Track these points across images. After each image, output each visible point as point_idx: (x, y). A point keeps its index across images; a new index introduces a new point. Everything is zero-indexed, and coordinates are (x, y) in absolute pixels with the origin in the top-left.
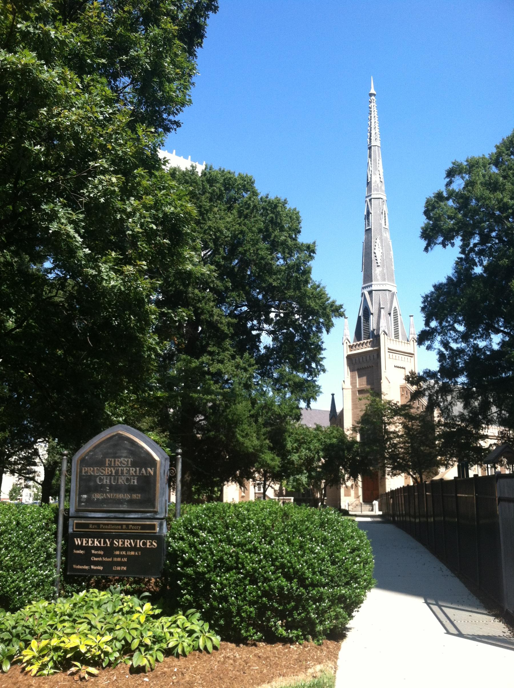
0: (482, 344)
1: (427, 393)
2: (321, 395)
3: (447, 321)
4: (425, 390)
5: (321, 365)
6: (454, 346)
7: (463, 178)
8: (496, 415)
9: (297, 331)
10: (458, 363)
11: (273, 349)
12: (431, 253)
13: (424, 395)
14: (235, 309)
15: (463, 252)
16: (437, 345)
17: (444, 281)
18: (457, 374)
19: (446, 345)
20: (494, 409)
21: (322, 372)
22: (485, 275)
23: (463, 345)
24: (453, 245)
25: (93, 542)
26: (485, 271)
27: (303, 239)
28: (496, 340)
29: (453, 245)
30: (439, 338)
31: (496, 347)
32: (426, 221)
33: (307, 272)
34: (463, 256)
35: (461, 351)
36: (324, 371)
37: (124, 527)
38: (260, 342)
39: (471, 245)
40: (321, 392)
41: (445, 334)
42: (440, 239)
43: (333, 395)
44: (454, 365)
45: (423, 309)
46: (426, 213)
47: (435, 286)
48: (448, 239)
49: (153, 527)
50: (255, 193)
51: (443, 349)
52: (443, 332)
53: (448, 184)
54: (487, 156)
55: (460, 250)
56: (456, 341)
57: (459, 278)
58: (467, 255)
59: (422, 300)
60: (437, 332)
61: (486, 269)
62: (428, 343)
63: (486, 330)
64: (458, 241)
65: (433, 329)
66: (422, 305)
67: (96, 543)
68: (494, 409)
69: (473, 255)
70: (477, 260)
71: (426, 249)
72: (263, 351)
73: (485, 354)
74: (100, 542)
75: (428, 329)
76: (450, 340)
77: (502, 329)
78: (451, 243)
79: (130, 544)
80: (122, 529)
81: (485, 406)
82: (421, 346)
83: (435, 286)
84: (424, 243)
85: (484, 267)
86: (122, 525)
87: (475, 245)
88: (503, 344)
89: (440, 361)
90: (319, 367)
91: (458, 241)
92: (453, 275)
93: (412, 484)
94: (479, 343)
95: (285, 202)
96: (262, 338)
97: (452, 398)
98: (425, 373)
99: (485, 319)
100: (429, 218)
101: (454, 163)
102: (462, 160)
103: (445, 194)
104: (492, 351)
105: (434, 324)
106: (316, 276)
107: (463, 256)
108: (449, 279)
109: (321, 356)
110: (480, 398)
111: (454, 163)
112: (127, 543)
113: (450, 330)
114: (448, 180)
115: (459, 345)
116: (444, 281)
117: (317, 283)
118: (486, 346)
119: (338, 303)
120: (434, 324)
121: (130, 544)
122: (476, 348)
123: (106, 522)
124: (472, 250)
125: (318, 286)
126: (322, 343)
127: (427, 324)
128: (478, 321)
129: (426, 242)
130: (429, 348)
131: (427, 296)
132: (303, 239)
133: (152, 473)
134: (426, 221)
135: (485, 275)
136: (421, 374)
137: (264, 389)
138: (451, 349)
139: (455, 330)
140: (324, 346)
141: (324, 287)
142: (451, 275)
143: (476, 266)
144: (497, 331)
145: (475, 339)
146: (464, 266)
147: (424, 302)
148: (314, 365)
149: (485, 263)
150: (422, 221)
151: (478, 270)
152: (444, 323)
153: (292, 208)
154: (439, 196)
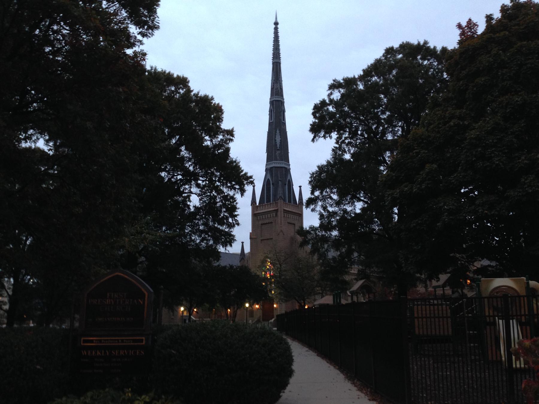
0: (349, 208)
1: (311, 242)
2: (235, 242)
3: (326, 192)
4: (309, 240)
5: (236, 220)
6: (330, 209)
7: (339, 91)
8: (357, 258)
9: (218, 194)
10: (333, 221)
11: (201, 208)
12: (316, 143)
13: (309, 244)
14: (172, 177)
15: (337, 142)
16: (319, 208)
17: (325, 163)
18: (331, 230)
19: (325, 208)
20: (356, 254)
21: (236, 226)
22: (352, 160)
23: (337, 209)
24: (331, 137)
25: (96, 353)
26: (352, 158)
27: (225, 126)
28: (359, 206)
29: (331, 137)
30: (320, 203)
31: (358, 211)
32: (314, 120)
33: (228, 150)
34: (337, 146)
35: (334, 213)
36: (238, 224)
37: (120, 341)
38: (190, 201)
39: (343, 139)
40: (235, 240)
41: (325, 201)
42: (322, 133)
43: (243, 243)
44: (330, 222)
45: (310, 182)
46: (314, 114)
47: (318, 167)
48: (328, 132)
49: (142, 341)
50: (189, 91)
51: (323, 211)
52: (324, 199)
53: (329, 95)
54: (357, 77)
55: (335, 141)
56: (331, 206)
57: (335, 162)
58: (340, 146)
59: (310, 176)
60: (319, 199)
61: (353, 156)
62: (312, 207)
63: (351, 199)
64: (334, 135)
65: (316, 197)
66: (310, 180)
67: (98, 353)
68: (356, 254)
69: (344, 146)
70: (347, 150)
71: (313, 140)
72: (192, 209)
73: (350, 216)
74: (101, 353)
75: (313, 196)
76: (328, 205)
77: (362, 198)
78: (329, 136)
79: (124, 353)
80: (118, 342)
81: (350, 252)
82: (308, 209)
83: (318, 167)
84: (311, 136)
85: (351, 154)
86: (118, 340)
87: (346, 138)
88: (363, 209)
89: (320, 219)
90: (234, 222)
91: (334, 135)
92: (331, 159)
93: (297, 308)
94: (347, 208)
95: (212, 99)
96: (191, 198)
97: (328, 246)
98: (310, 228)
99: (351, 192)
100: (315, 117)
101: (334, 81)
102: (340, 79)
103: (327, 101)
104: (355, 214)
105: (317, 193)
106: (233, 154)
107: (337, 146)
108: (328, 162)
109: (236, 213)
110: (346, 246)
111: (334, 81)
112: (122, 353)
113: (328, 198)
114: (329, 92)
115: (333, 209)
116: (325, 163)
117: (234, 160)
118: (351, 210)
119: (249, 175)
120: (317, 193)
121: (124, 353)
122: (345, 211)
123: (114, 338)
124: (343, 142)
125: (235, 161)
126: (237, 203)
127: (312, 193)
128: (348, 193)
129: (313, 135)
130: (313, 210)
131: (313, 174)
132: (225, 126)
133: (142, 303)
134: (314, 120)
135: (352, 160)
136: (308, 229)
137: (193, 238)
138: (328, 211)
139: (331, 198)
140: (238, 206)
141: (239, 163)
142: (329, 160)
143: (346, 153)
144: (359, 200)
145: (344, 205)
146: (337, 152)
147: (311, 177)
148: (230, 220)
149: (352, 152)
150: (311, 120)
151: (347, 156)
152: (324, 193)
153: (217, 103)
154: (323, 103)
